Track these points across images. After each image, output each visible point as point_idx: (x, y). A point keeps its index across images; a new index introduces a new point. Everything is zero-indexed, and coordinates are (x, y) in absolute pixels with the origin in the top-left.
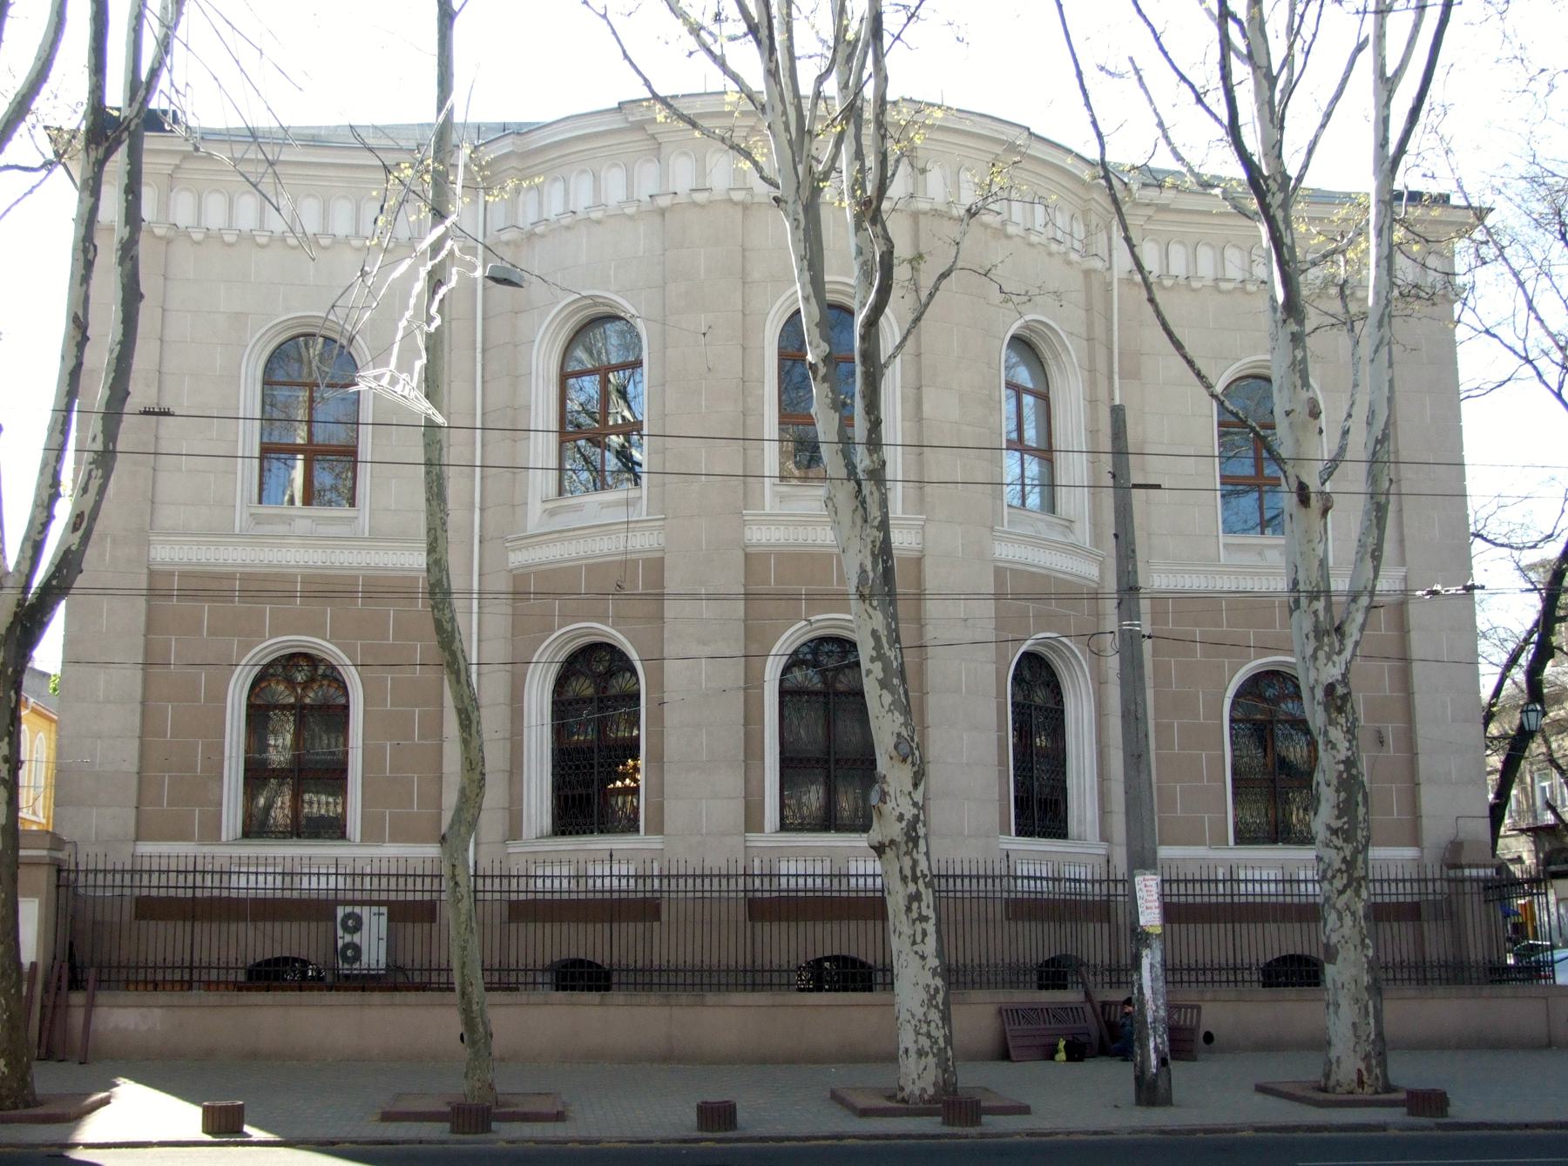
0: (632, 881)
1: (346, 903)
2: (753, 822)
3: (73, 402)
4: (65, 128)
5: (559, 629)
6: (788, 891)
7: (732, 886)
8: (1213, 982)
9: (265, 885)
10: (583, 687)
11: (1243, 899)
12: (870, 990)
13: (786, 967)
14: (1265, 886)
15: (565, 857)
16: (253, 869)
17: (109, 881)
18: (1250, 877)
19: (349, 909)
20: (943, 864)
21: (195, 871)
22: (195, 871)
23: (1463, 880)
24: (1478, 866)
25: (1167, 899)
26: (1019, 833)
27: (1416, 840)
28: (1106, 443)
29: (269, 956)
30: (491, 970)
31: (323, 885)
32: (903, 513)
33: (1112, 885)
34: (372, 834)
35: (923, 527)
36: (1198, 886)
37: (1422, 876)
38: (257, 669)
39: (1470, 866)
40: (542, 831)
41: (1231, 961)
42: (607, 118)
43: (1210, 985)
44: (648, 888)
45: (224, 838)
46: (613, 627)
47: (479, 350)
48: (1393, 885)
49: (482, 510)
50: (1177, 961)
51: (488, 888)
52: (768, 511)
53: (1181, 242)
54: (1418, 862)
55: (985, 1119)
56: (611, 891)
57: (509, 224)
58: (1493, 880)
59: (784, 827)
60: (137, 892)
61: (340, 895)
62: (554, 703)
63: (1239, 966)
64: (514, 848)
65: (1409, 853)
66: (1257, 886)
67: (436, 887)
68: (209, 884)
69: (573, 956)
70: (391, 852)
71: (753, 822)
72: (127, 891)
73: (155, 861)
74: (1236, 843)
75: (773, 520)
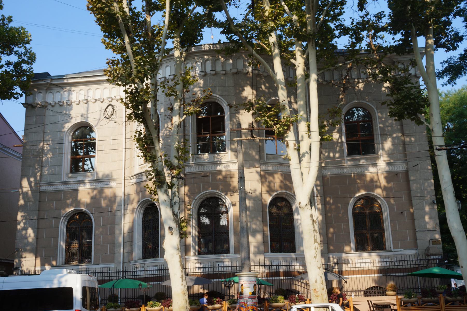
6: (206, 272)
8: (359, 295)
11: (148, 276)
13: (399, 288)
18: (154, 269)
20: (127, 268)
21: (410, 260)
22: (410, 260)
23: (431, 259)
24: (435, 255)
25: (99, 279)
26: (271, 252)
27: (416, 246)
28: (296, 130)
30: (270, 294)
31: (207, 271)
32: (231, 159)
38: (69, 217)
39: (433, 255)
40: (139, 257)
41: (412, 286)
43: (360, 296)
50: (133, 296)
51: (113, 275)
52: (265, 161)
54: (416, 255)
56: (219, 271)
62: (143, 221)
63: (415, 288)
65: (413, 252)
68: (396, 265)
70: (401, 253)
74: (271, 252)
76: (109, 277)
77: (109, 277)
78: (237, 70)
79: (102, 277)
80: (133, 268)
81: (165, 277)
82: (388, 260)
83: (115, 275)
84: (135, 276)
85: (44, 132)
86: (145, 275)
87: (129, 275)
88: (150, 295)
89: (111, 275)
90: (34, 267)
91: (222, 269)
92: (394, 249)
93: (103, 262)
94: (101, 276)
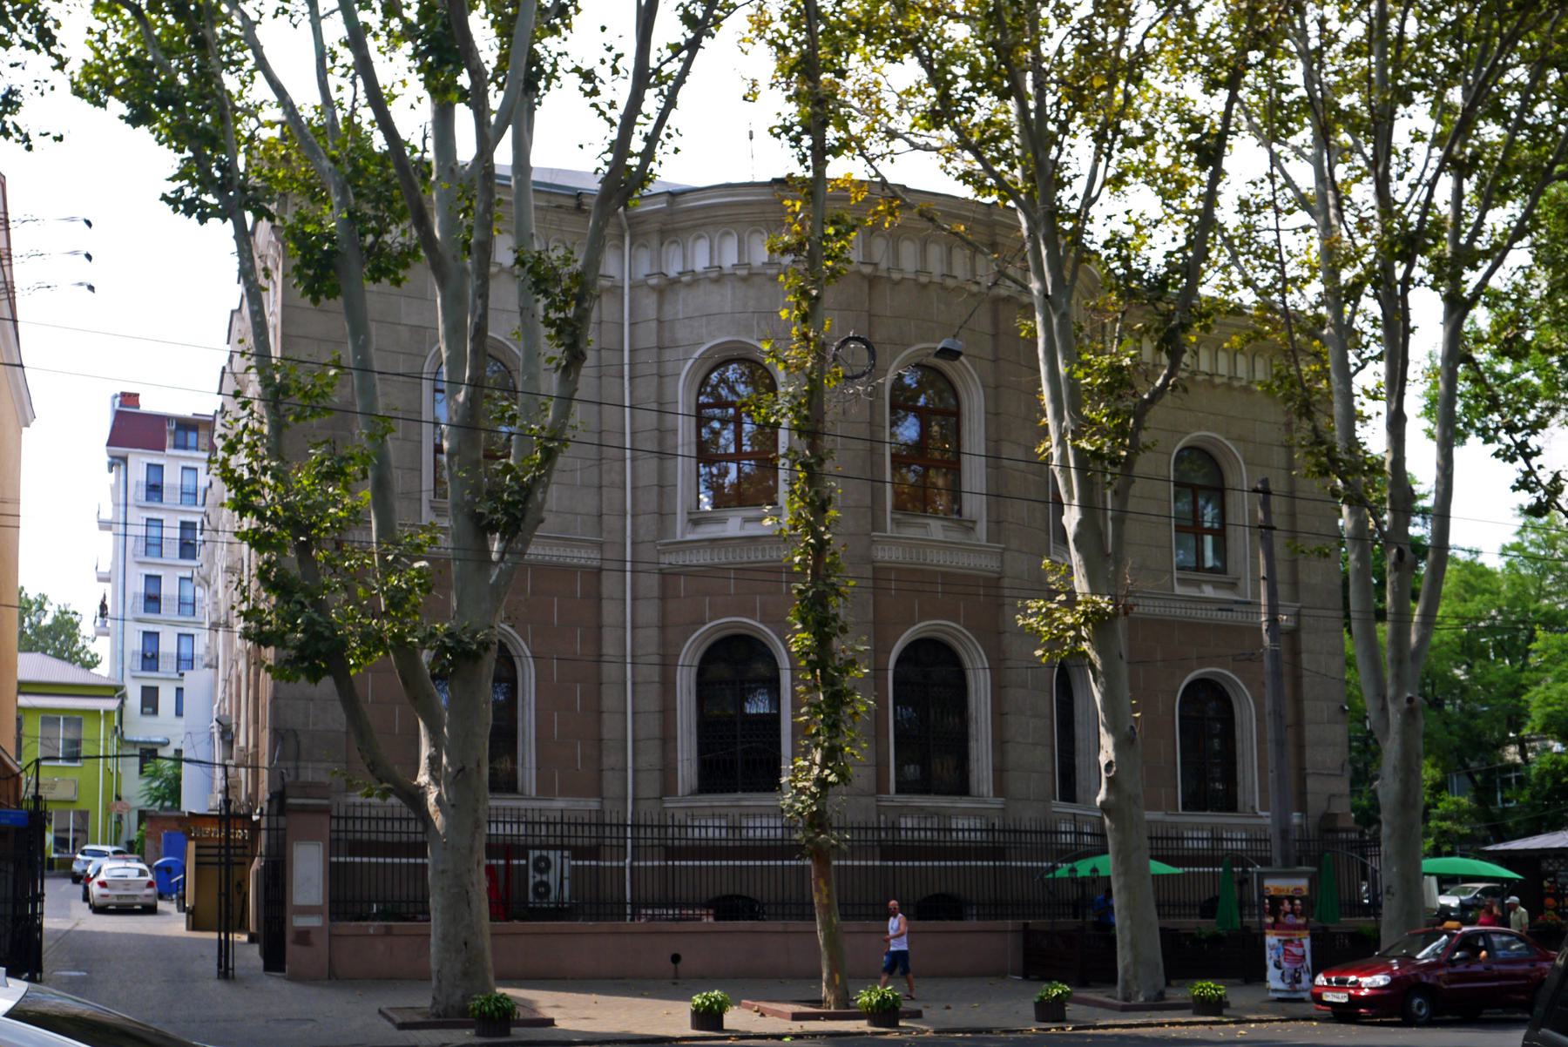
0: (724, 831)
1: (534, 848)
2: (881, 787)
3: (555, 419)
4: (1307, 286)
5: (711, 620)
7: (870, 837)
9: (713, 832)
10: (720, 671)
12: (491, 920)
14: (973, 834)
15: (723, 811)
16: (501, 819)
17: (358, 827)
19: (537, 853)
20: (614, 815)
26: (1062, 799)
29: (931, 893)
32: (988, 541)
33: (565, 827)
34: (545, 790)
35: (1002, 555)
36: (404, 823)
37: (662, 823)
42: (767, 190)
44: (948, 839)
45: (680, 793)
46: (761, 622)
47: (626, 378)
48: (573, 828)
49: (633, 516)
52: (889, 534)
53: (1206, 347)
55: (514, 1030)
56: (783, 840)
57: (655, 271)
58: (1355, 841)
59: (898, 791)
60: (350, 836)
61: (530, 840)
64: (669, 804)
66: (960, 834)
67: (662, 836)
69: (724, 892)
71: (881, 787)
72: (342, 835)
73: (529, 814)
74: (1184, 808)
75: (894, 541)
76: (673, 839)
77: (673, 839)
78: (750, 269)
79: (370, 832)
80: (737, 817)
81: (608, 849)
82: (723, 824)
83: (586, 833)
84: (362, 832)
85: (661, 515)
86: (562, 837)
87: (601, 834)
88: (759, 894)
89: (566, 833)
90: (41, 781)
91: (922, 833)
92: (1262, 810)
93: (564, 793)
94: (365, 828)
